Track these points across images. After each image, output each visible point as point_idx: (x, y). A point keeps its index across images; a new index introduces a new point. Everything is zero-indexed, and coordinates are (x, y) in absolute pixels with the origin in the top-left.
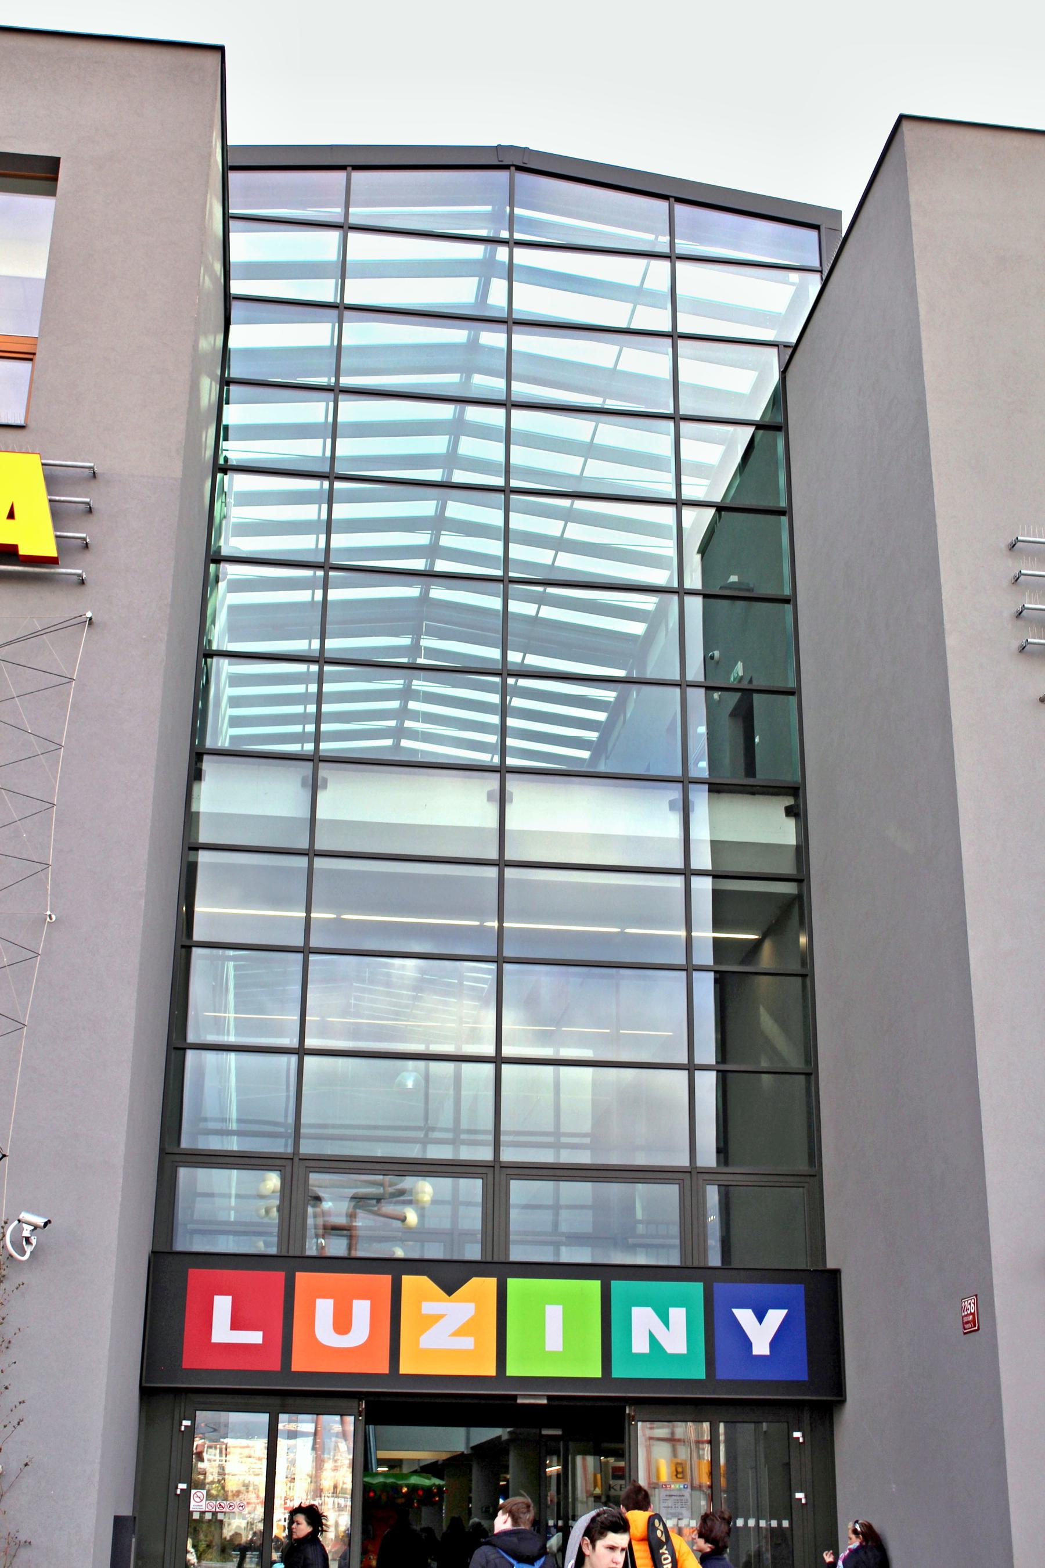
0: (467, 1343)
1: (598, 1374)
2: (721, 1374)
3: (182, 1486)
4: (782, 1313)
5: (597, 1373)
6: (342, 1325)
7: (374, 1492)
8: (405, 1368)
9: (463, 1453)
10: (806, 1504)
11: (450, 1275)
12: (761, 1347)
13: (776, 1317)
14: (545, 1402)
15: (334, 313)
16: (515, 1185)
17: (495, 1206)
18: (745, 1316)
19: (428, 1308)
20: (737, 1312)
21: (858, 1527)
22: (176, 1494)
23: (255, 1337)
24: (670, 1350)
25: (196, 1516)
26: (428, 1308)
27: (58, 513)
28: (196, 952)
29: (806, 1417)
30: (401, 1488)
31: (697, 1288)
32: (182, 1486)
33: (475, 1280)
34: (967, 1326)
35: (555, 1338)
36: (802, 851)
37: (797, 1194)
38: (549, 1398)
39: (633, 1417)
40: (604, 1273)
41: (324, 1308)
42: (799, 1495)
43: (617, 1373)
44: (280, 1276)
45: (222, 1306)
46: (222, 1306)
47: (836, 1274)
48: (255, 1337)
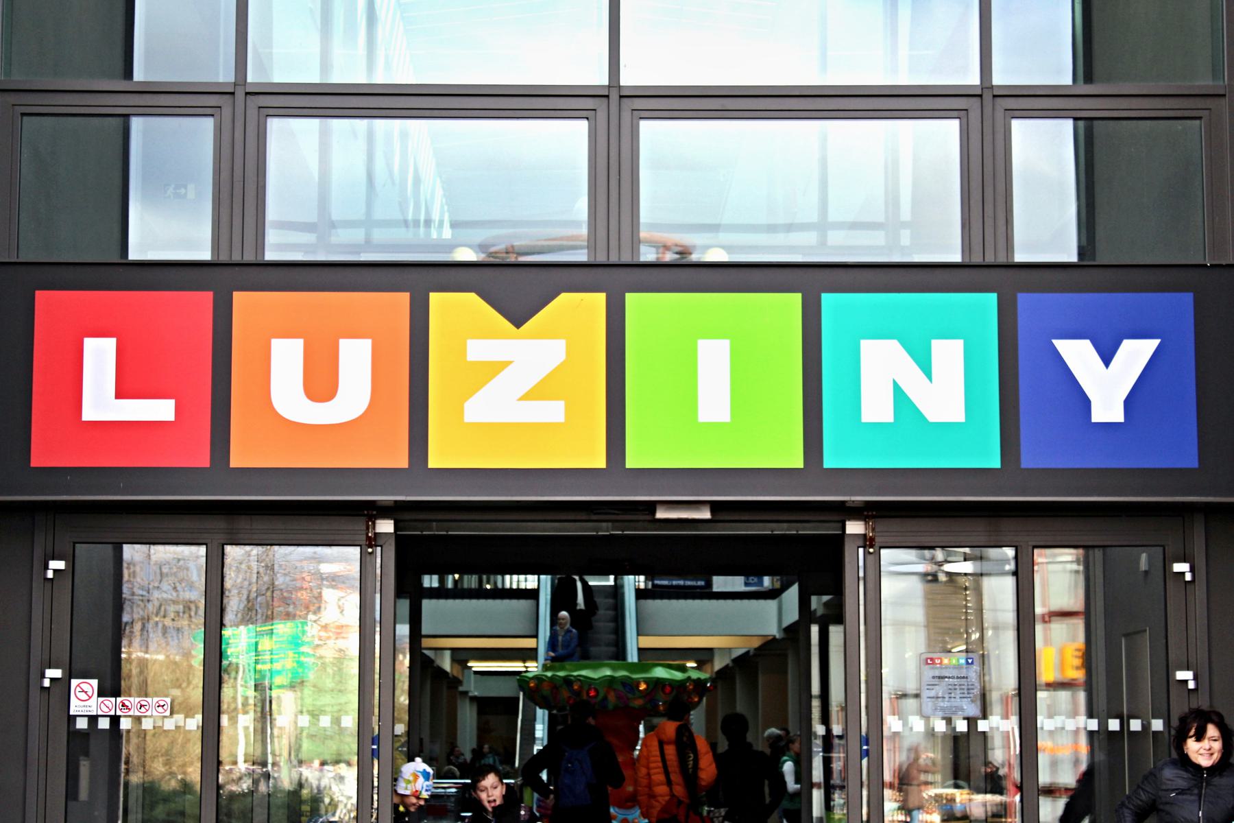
0: (552, 411)
3: (56, 673)
4: (1148, 347)
5: (796, 460)
6: (321, 382)
7: (597, 691)
9: (774, 639)
10: (1196, 690)
11: (516, 284)
12: (1108, 406)
13: (1136, 354)
14: (706, 515)
17: (614, 177)
18: (1077, 354)
19: (478, 350)
20: (1062, 345)
22: (43, 688)
23: (162, 410)
24: (934, 414)
25: (82, 724)
28: (627, 79)
30: (638, 685)
32: (56, 673)
33: (565, 299)
35: (715, 404)
38: (715, 507)
39: (872, 540)
40: (812, 279)
41: (287, 358)
44: (206, 299)
45: (100, 355)
46: (100, 355)
48: (162, 410)
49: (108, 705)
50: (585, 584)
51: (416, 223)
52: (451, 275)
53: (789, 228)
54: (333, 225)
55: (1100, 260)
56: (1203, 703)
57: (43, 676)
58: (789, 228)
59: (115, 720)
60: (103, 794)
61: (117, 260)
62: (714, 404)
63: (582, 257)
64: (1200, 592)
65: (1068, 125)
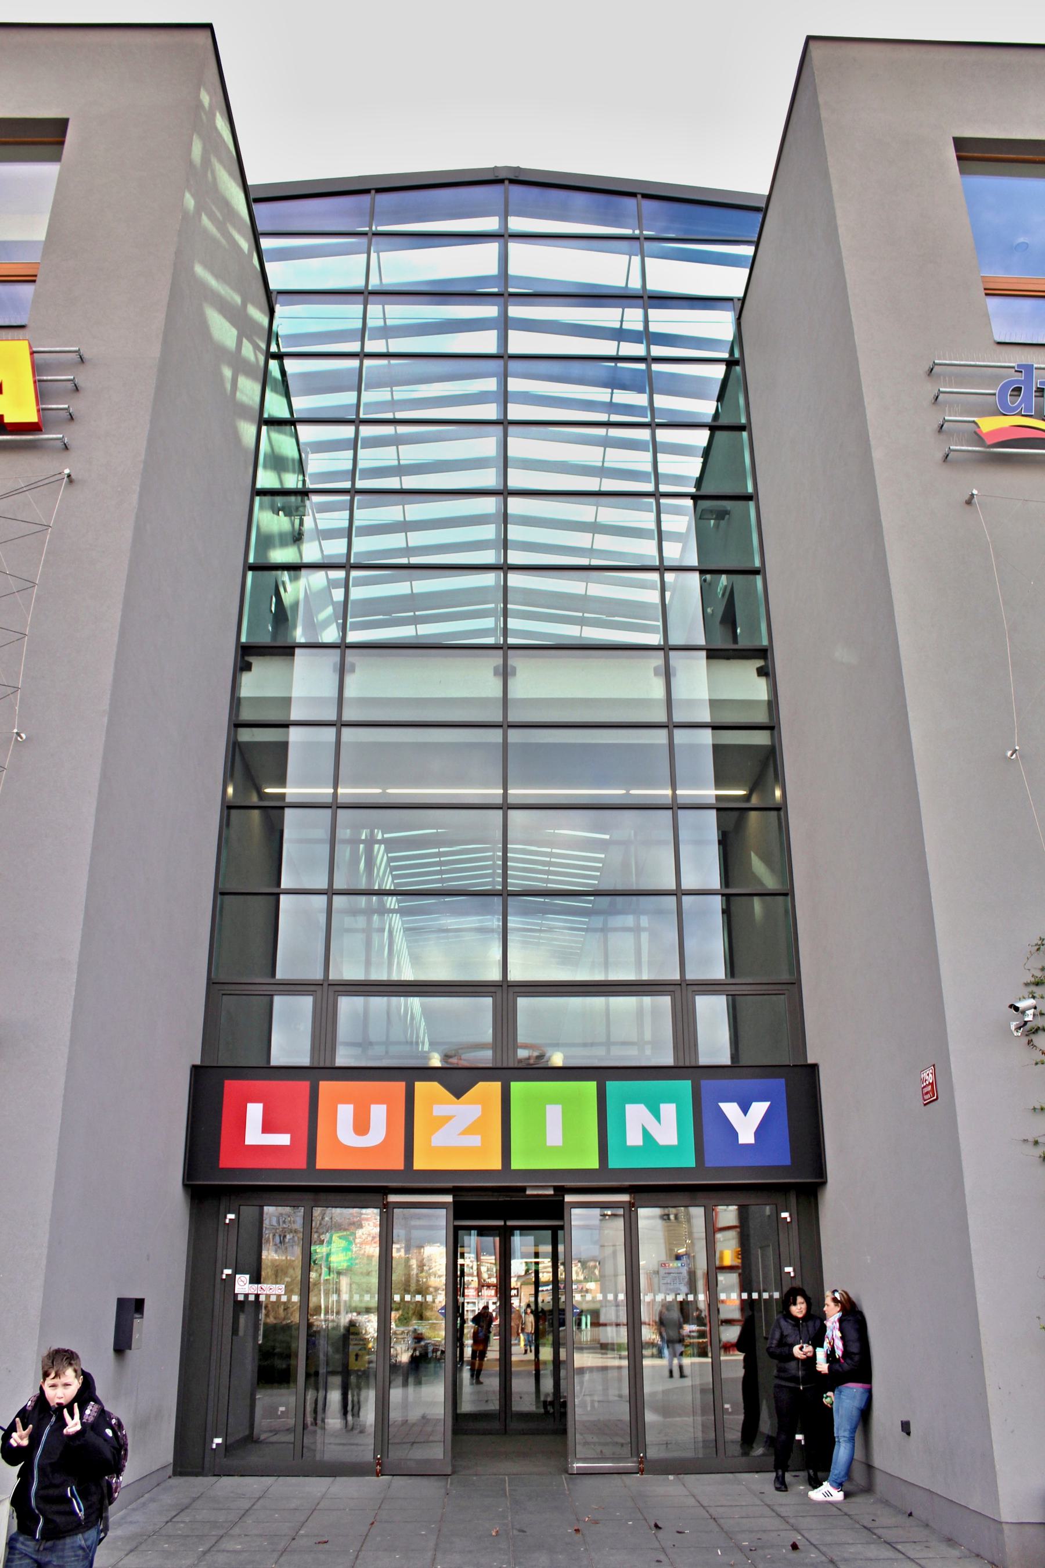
0: (475, 1141)
1: (595, 1165)
2: (710, 1162)
3: (228, 1272)
6: (362, 1126)
8: (418, 1165)
11: (458, 1078)
12: (746, 1136)
13: (759, 1109)
14: (552, 1192)
15: (361, 298)
16: (522, 1002)
17: (505, 1021)
18: (731, 1109)
19: (439, 1110)
21: (837, 1295)
23: (283, 1139)
25: (241, 1298)
26: (439, 1110)
27: (41, 395)
29: (793, 1200)
31: (685, 1086)
32: (228, 1272)
33: (481, 1085)
34: (926, 1097)
36: (773, 705)
37: (781, 1001)
38: (556, 1188)
40: (601, 1074)
41: (345, 1113)
42: (788, 1269)
43: (613, 1163)
46: (255, 1112)
47: (814, 1067)
48: (283, 1139)
49: (254, 1289)
50: (383, 1405)
51: (411, 1043)
52: (427, 1073)
53: (592, 1045)
54: (371, 1044)
55: (741, 1064)
56: (798, 1283)
57: (222, 1273)
58: (592, 1045)
59: (257, 1296)
60: (250, 1331)
61: (263, 1064)
62: (554, 1136)
63: (490, 1065)
64: (795, 1223)
65: (724, 998)
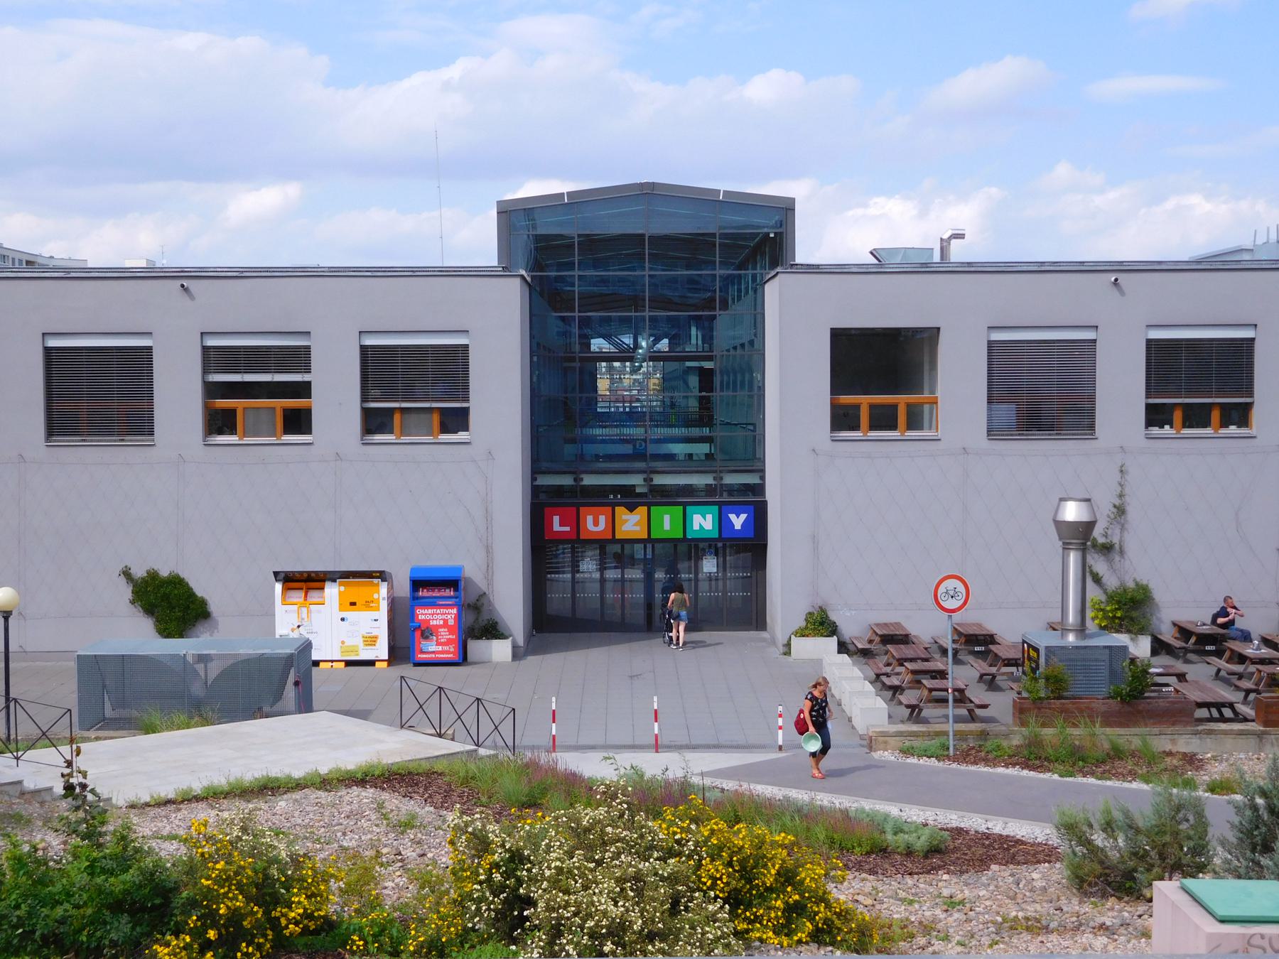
6: (596, 523)
12: (738, 526)
13: (743, 517)
18: (732, 517)
23: (568, 529)
26: (624, 517)
41: (590, 519)
46: (556, 519)
48: (568, 529)
